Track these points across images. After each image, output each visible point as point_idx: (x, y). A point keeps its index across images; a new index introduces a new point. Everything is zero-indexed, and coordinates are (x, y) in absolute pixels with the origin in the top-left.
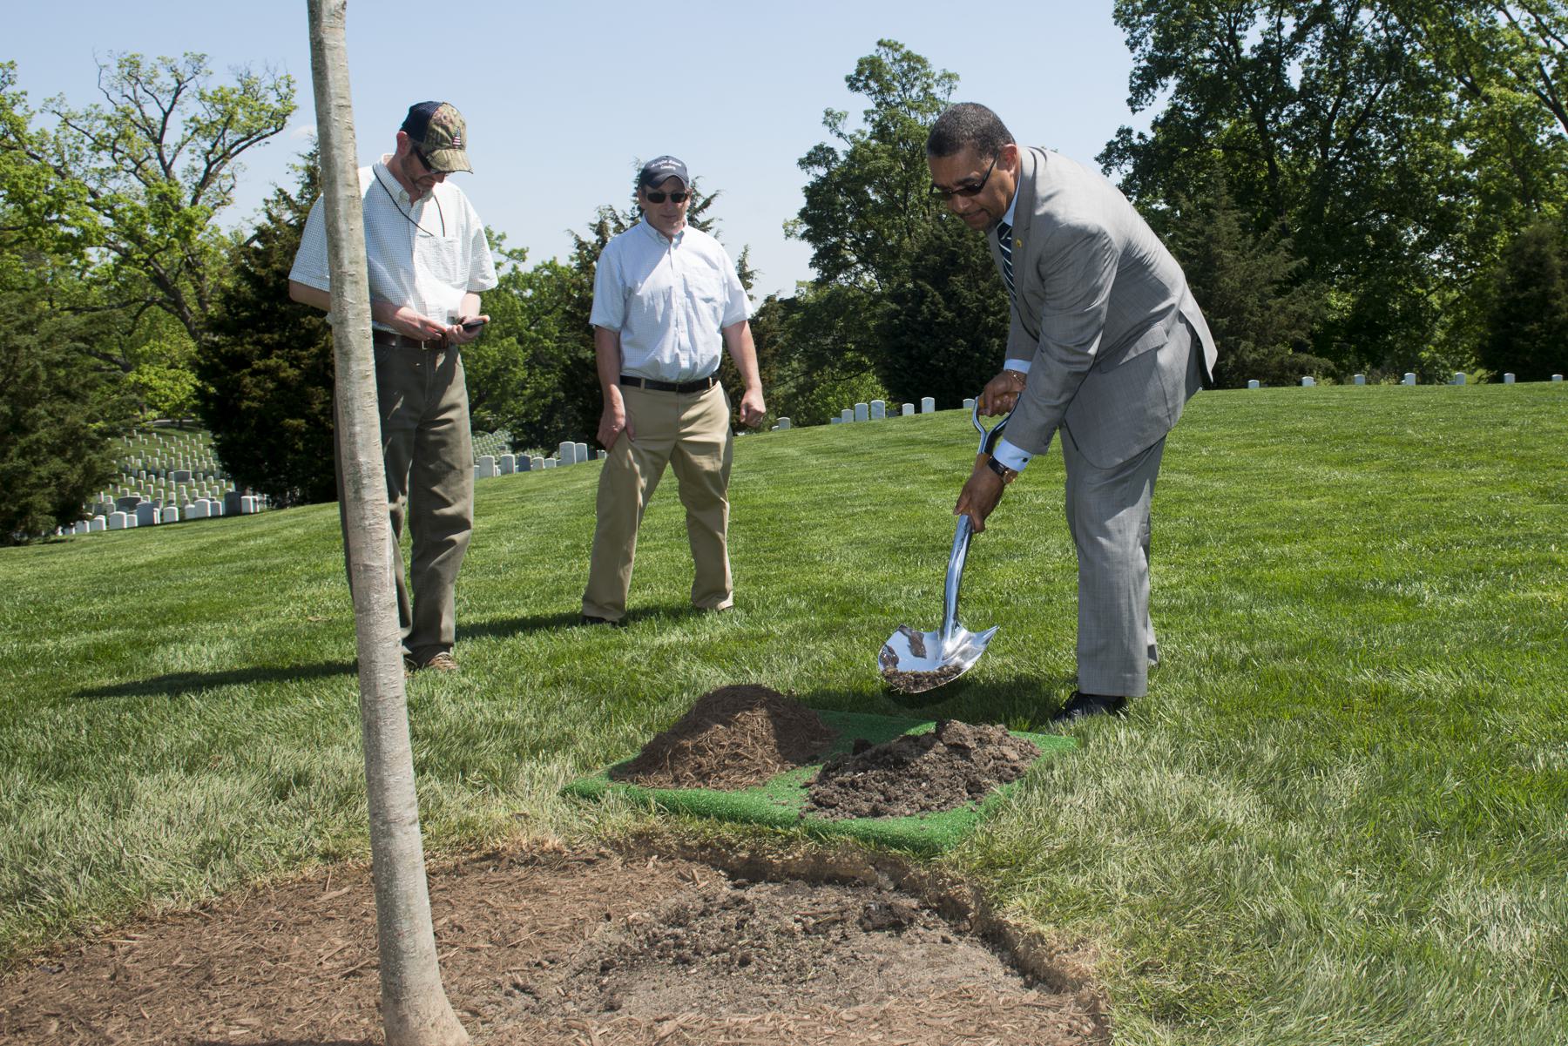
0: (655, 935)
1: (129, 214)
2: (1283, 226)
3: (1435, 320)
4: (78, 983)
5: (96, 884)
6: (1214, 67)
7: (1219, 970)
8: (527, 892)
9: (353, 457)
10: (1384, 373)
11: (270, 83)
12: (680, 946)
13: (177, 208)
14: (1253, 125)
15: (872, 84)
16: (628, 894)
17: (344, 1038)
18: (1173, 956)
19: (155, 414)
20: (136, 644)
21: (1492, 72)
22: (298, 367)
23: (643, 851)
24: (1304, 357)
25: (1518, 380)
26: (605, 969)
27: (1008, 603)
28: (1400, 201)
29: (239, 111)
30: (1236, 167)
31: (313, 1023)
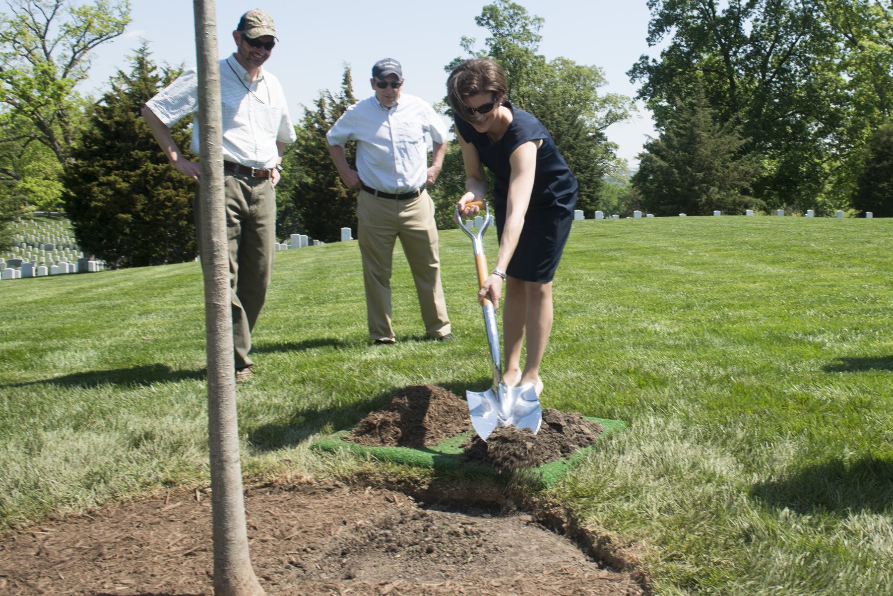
0: (373, 534)
1: (22, 82)
2: (737, 119)
3: (826, 178)
4: (16, 557)
5: (23, 497)
6: (699, 21)
7: (716, 560)
8: (293, 507)
9: (210, 238)
10: (794, 209)
11: (115, 4)
12: (388, 541)
13: (53, 80)
14: (722, 57)
15: (491, 22)
16: (356, 509)
17: (188, 592)
18: (688, 551)
19: (33, 208)
20: (33, 350)
21: (864, 32)
22: (129, 182)
23: (363, 483)
24: (747, 198)
25: (874, 216)
26: (344, 554)
27: (577, 340)
28: (808, 106)
29: (95, 20)
30: (711, 82)
31: (168, 584)
